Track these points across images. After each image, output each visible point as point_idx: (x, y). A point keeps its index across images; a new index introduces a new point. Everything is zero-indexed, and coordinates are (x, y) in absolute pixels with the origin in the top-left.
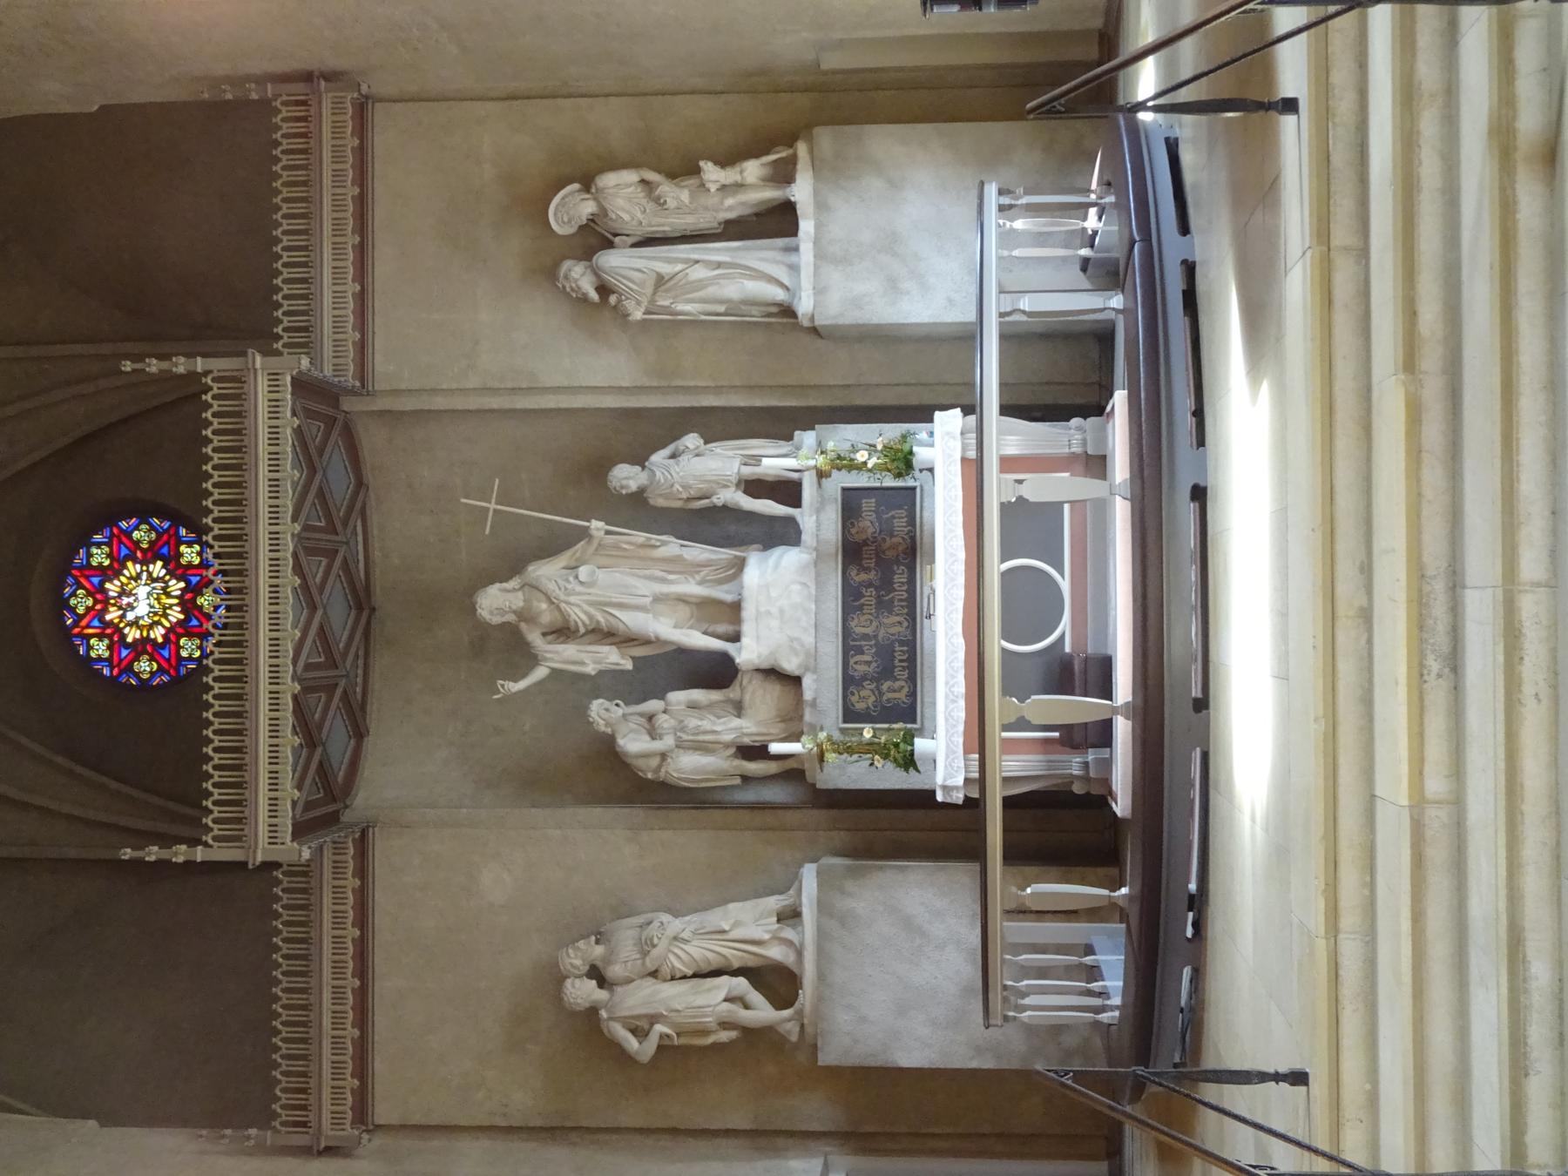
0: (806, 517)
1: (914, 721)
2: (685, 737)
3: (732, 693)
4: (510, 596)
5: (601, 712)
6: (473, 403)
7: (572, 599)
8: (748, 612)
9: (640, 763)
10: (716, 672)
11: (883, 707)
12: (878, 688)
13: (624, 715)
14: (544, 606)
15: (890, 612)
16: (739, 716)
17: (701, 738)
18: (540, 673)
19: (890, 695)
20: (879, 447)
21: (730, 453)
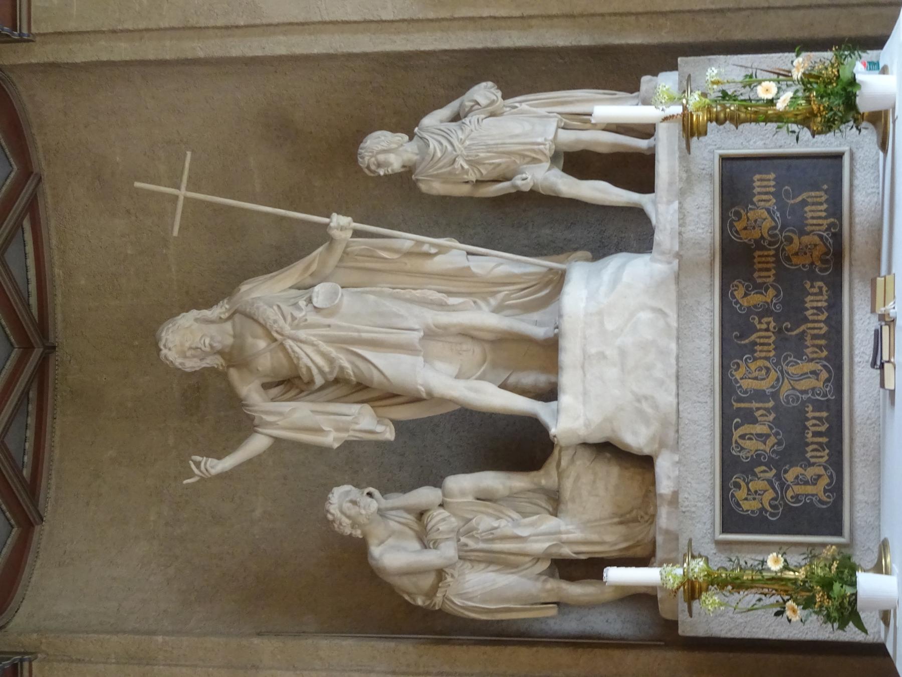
0: (661, 207)
1: (839, 532)
2: (472, 544)
3: (546, 478)
4: (213, 329)
5: (347, 504)
6: (169, 49)
7: (302, 334)
8: (569, 355)
9: (405, 583)
10: (520, 446)
11: (788, 508)
12: (778, 476)
13: (381, 513)
14: (262, 344)
15: (800, 355)
16: (555, 513)
17: (498, 546)
18: (257, 444)
19: (799, 489)
20: (797, 74)
21: (543, 111)
